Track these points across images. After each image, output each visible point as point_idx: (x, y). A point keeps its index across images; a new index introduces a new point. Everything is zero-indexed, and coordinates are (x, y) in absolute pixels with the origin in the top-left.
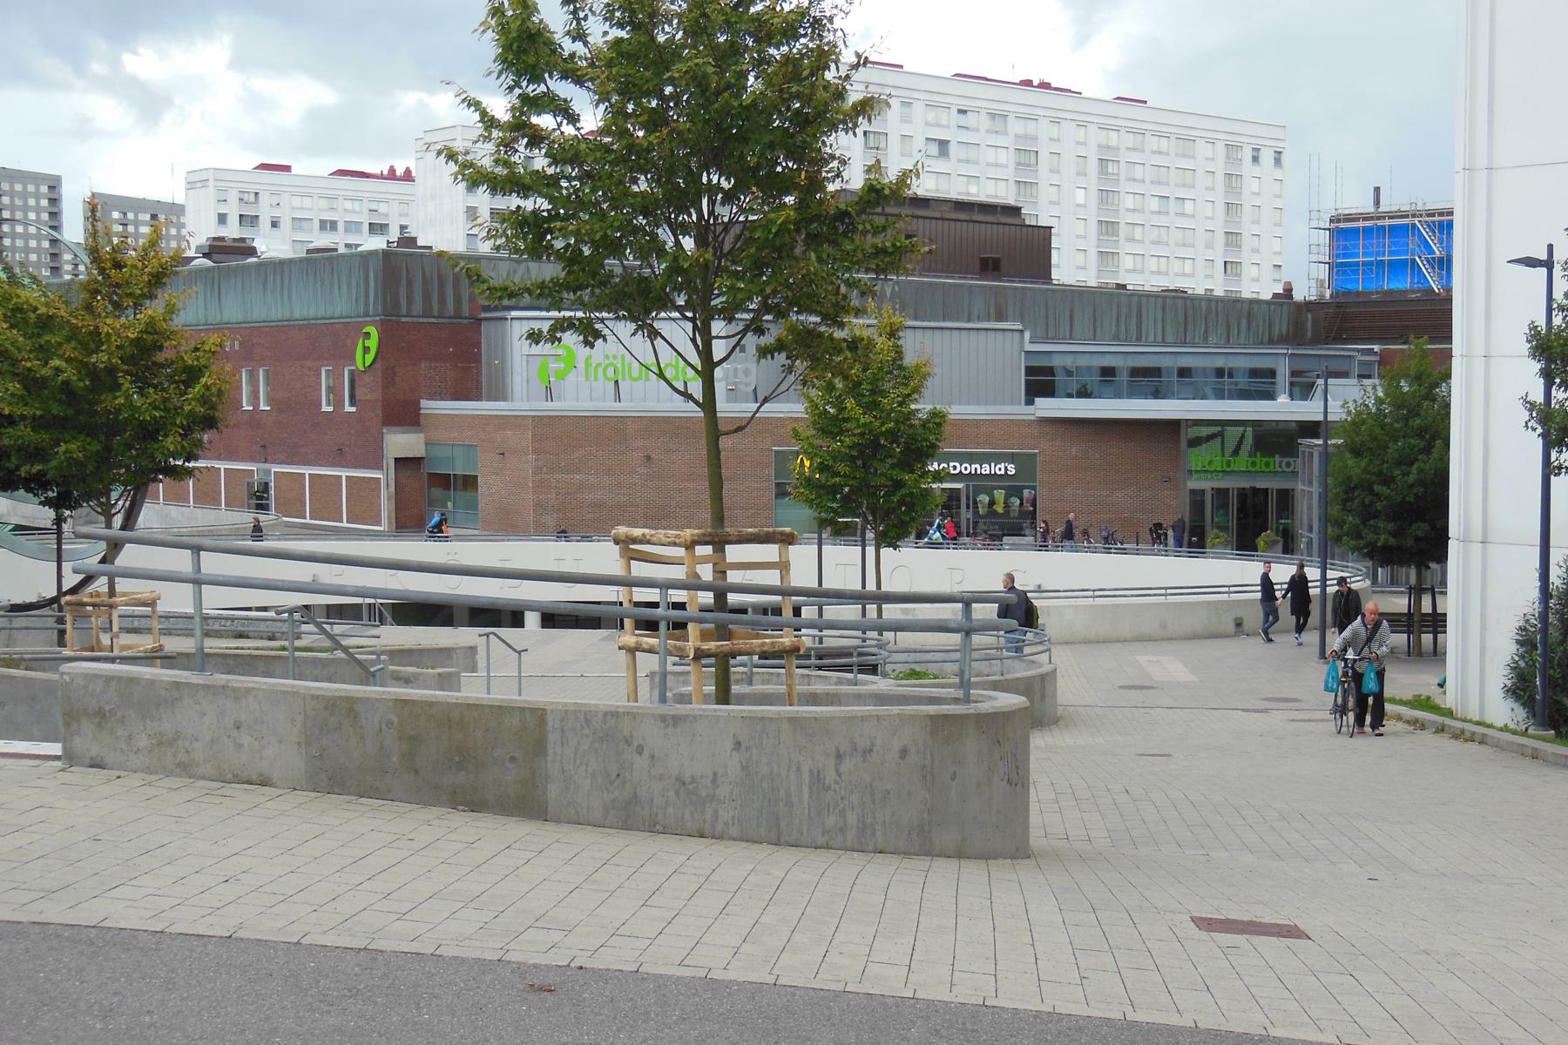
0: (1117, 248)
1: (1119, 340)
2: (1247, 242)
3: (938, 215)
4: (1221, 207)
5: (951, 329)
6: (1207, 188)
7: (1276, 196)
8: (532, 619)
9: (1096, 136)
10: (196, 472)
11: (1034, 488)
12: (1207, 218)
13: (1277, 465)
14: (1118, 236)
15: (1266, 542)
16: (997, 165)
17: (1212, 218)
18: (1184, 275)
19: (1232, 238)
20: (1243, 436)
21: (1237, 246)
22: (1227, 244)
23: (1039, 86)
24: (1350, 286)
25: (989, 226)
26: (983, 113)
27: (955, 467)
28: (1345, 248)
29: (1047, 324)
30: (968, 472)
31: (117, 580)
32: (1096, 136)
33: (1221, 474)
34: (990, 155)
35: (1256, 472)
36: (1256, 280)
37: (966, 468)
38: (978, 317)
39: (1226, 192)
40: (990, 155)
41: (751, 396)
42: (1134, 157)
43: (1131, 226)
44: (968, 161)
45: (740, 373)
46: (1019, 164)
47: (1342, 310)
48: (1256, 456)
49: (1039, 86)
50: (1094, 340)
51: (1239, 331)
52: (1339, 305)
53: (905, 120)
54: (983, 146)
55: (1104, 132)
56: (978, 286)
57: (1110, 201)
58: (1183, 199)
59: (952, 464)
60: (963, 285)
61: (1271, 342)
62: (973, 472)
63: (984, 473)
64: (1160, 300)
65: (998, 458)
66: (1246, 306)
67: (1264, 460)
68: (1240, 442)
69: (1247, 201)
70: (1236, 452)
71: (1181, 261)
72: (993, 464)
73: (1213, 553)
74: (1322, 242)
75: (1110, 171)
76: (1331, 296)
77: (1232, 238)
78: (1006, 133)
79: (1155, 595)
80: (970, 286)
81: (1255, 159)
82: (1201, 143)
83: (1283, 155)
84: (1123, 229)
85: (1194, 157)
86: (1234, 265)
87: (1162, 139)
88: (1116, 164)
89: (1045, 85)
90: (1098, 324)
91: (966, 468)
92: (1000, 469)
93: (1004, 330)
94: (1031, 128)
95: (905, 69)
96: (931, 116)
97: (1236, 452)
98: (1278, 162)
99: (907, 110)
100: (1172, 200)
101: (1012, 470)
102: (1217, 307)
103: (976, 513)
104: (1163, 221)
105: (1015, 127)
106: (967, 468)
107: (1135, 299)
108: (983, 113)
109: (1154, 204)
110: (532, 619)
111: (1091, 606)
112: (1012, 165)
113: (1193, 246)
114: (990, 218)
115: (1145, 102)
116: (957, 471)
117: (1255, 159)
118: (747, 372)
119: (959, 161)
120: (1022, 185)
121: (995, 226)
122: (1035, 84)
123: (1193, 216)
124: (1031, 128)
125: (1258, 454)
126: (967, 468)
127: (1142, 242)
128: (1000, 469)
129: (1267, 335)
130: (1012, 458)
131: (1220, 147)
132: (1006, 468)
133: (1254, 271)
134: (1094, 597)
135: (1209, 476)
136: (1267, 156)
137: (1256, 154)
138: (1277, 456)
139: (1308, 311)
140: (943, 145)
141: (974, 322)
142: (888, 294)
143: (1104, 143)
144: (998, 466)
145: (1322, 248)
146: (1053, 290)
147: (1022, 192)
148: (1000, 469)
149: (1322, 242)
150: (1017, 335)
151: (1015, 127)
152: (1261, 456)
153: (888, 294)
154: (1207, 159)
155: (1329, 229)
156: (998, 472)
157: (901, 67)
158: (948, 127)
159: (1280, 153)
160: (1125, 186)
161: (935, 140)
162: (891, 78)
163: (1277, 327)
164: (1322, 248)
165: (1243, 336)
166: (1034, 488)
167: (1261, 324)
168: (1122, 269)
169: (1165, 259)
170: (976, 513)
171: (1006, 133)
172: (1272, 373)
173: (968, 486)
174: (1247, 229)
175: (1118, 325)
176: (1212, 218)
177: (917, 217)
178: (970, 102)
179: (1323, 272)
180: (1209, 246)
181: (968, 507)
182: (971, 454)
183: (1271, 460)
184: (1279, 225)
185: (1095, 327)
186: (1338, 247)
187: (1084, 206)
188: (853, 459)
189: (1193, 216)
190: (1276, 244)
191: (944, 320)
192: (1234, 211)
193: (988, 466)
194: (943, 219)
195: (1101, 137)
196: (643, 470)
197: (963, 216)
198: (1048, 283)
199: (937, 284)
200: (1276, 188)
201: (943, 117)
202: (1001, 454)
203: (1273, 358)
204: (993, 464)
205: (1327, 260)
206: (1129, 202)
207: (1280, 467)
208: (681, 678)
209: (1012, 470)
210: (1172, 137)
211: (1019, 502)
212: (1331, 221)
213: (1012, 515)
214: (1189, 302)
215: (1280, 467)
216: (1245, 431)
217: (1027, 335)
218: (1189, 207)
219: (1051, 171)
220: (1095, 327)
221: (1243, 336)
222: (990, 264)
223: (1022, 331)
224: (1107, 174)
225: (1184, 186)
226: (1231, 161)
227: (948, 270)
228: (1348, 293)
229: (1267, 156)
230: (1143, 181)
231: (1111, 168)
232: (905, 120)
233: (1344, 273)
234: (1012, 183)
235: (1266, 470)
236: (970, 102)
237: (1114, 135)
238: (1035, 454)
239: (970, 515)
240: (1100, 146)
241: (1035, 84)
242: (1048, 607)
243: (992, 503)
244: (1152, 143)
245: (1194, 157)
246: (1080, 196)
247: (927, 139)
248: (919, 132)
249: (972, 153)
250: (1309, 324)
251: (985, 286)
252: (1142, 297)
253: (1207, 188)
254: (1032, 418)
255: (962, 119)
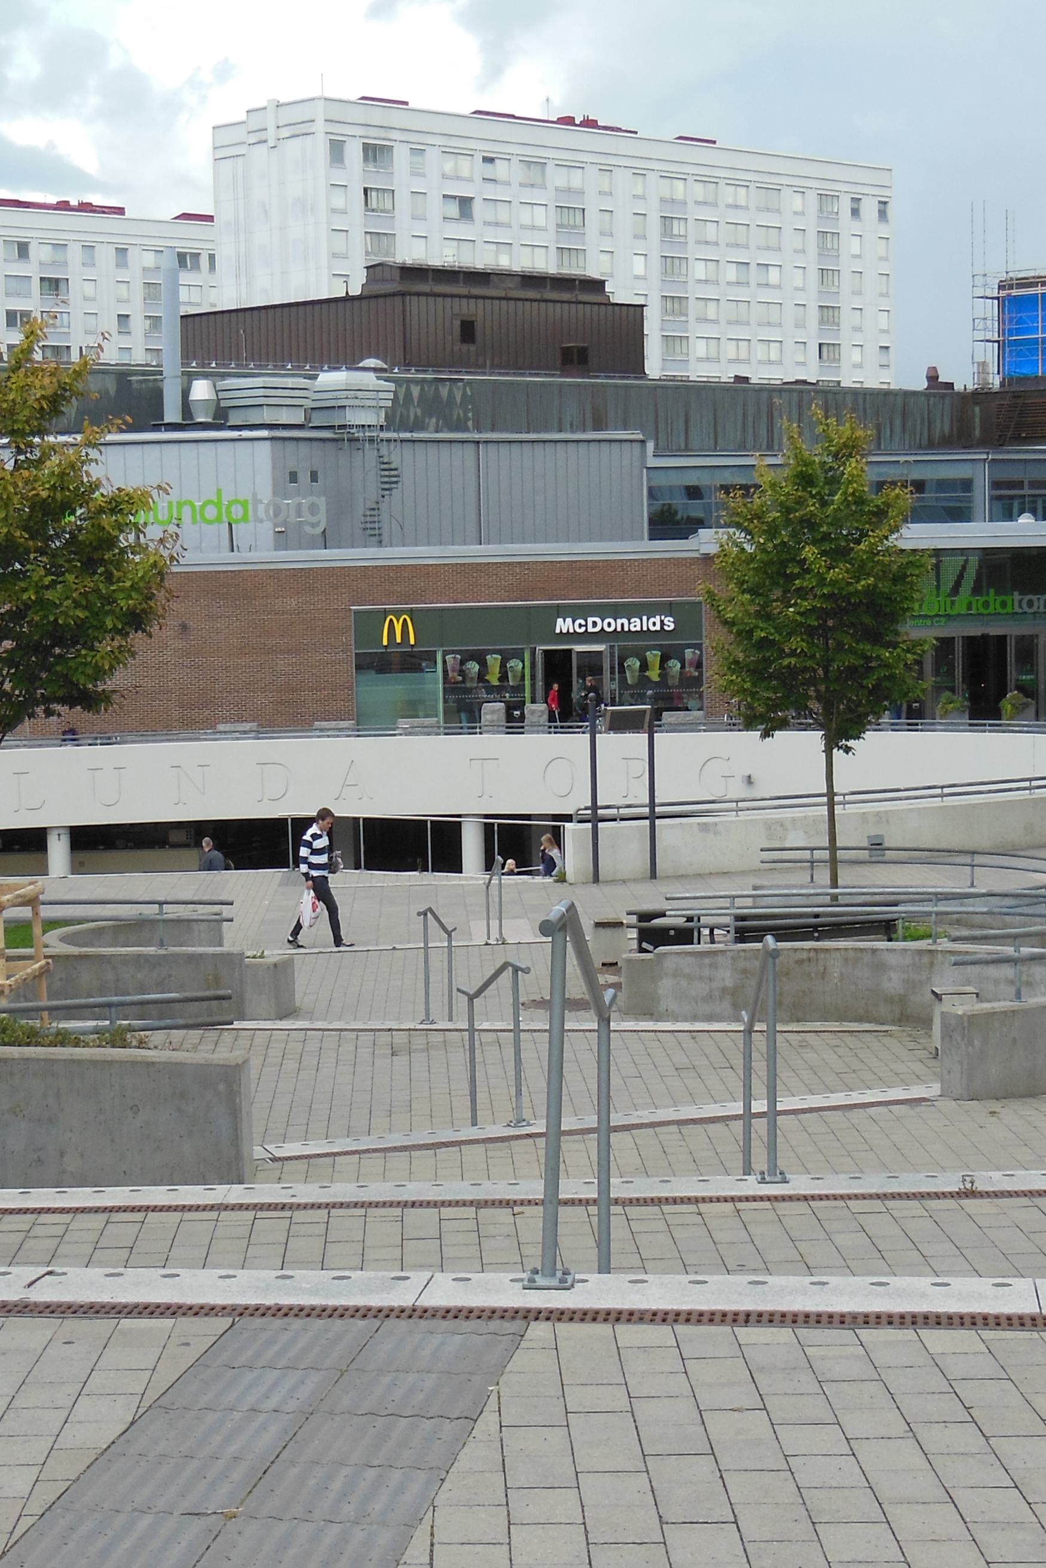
0: (686, 331)
1: (745, 449)
2: (847, 318)
3: (501, 293)
4: (814, 276)
5: (556, 442)
6: (796, 251)
7: (881, 259)
8: (58, 850)
9: (658, 189)
10: (115, 697)
11: (699, 647)
12: (797, 289)
13: (1016, 604)
14: (687, 315)
15: (1013, 705)
16: (533, 228)
17: (803, 289)
18: (770, 362)
19: (828, 314)
20: (964, 568)
21: (834, 323)
22: (822, 322)
23: (582, 125)
24: (1026, 371)
25: (566, 306)
26: (515, 160)
27: (595, 624)
28: (1020, 321)
29: (657, 428)
30: (612, 629)
31: (702, 929)
32: (658, 189)
33: (943, 620)
34: (525, 216)
35: (989, 614)
36: (859, 366)
37: (609, 625)
38: (571, 425)
39: (819, 255)
40: (525, 216)
41: (321, 540)
42: (704, 213)
43: (702, 303)
44: (497, 224)
45: (305, 510)
46: (559, 226)
47: (1020, 401)
48: (988, 594)
49: (582, 125)
50: (715, 450)
51: (891, 431)
52: (1016, 395)
53: (416, 173)
54: (515, 204)
55: (668, 181)
56: (570, 385)
57: (676, 271)
58: (767, 265)
59: (590, 620)
60: (551, 384)
61: (931, 445)
62: (619, 629)
63: (633, 629)
64: (795, 394)
65: (651, 610)
66: (899, 401)
67: (1000, 599)
68: (961, 576)
69: (846, 266)
70: (955, 590)
71: (764, 346)
72: (645, 618)
73: (990, 725)
74: (989, 315)
75: (676, 232)
76: (1002, 384)
77: (828, 314)
78: (543, 187)
79: (1018, 789)
80: (561, 385)
81: (855, 212)
82: (786, 192)
83: (889, 205)
84: (693, 308)
85: (778, 211)
86: (831, 348)
87: (739, 188)
88: (682, 222)
89: (589, 123)
90: (719, 429)
91: (609, 625)
92: (654, 624)
93: (621, 441)
94: (576, 179)
95: (411, 106)
96: (448, 166)
97: (955, 590)
98: (883, 214)
99: (419, 159)
100: (753, 267)
101: (670, 625)
102: (865, 401)
103: (623, 680)
104: (742, 294)
105: (557, 178)
106: (610, 624)
107: (765, 395)
108: (515, 160)
109: (731, 273)
110: (58, 850)
111: (941, 807)
112: (552, 228)
113: (780, 325)
114: (566, 296)
115: (714, 142)
116: (597, 629)
117: (855, 212)
118: (313, 509)
119: (485, 223)
120: (566, 253)
121: (573, 306)
122: (577, 122)
123: (779, 287)
124: (576, 179)
125: (992, 591)
126: (610, 624)
127: (715, 322)
128: (654, 624)
129: (926, 437)
130: (668, 609)
131: (812, 197)
132: (662, 622)
133: (856, 356)
134: (942, 796)
135: (929, 622)
136: (869, 208)
137: (856, 206)
138: (1016, 593)
139: (976, 404)
140: (465, 204)
141: (566, 431)
142: (458, 399)
143: (668, 196)
144: (652, 620)
145: (989, 323)
146: (647, 387)
147: (566, 262)
148: (653, 623)
149: (989, 315)
150: (637, 447)
151: (557, 178)
152: (997, 594)
153: (458, 399)
154: (795, 213)
155: (998, 298)
156: (652, 628)
157: (406, 103)
158: (471, 180)
159: (885, 203)
160: (693, 251)
161: (454, 197)
162: (396, 118)
163: (938, 424)
164: (989, 323)
165: (897, 439)
166: (699, 647)
167: (919, 422)
168: (691, 358)
169: (746, 343)
170: (623, 680)
171: (543, 187)
172: (967, 485)
173: (612, 647)
174: (846, 302)
175: (744, 429)
176: (803, 289)
177: (476, 297)
178: (499, 148)
179: (990, 355)
180: (800, 324)
181: (612, 672)
182: (616, 605)
183: (1008, 599)
184: (886, 295)
185: (716, 432)
186: (1011, 320)
187: (644, 278)
188: (811, 631)
189: (779, 287)
190: (883, 321)
191: (493, 430)
192: (830, 278)
193: (638, 620)
194: (546, 301)
195: (664, 188)
196: (179, 644)
197: (531, 294)
198: (641, 378)
199: (518, 383)
200: (881, 248)
201: (465, 166)
202: (589, 605)
203: (969, 465)
204: (645, 618)
205: (996, 338)
206: (699, 271)
207: (1020, 607)
208: (707, 961)
209: (670, 625)
210: (752, 186)
211: (679, 665)
212: (1001, 287)
213: (670, 682)
214: (830, 396)
215: (1020, 607)
216: (966, 561)
217: (650, 446)
218: (774, 276)
219: (602, 234)
220: (716, 432)
221: (897, 439)
222: (575, 357)
223: (643, 442)
224: (672, 236)
225: (768, 248)
226: (825, 215)
227: (518, 366)
228: (1021, 380)
229: (869, 208)
230: (717, 244)
231: (677, 228)
232: (416, 173)
233: (1019, 354)
234: (553, 251)
235: (985, 612)
236: (499, 148)
237: (680, 184)
238: (700, 603)
239: (615, 686)
240: (662, 200)
241: (577, 122)
242: (886, 812)
243: (644, 666)
244: (728, 195)
245: (778, 211)
246: (639, 266)
247: (444, 196)
248: (434, 187)
249: (503, 213)
250: (977, 420)
251: (579, 385)
252: (768, 391)
253: (796, 251)
254: (696, 555)
255: (488, 170)
